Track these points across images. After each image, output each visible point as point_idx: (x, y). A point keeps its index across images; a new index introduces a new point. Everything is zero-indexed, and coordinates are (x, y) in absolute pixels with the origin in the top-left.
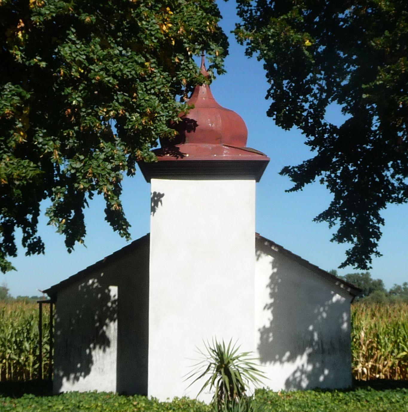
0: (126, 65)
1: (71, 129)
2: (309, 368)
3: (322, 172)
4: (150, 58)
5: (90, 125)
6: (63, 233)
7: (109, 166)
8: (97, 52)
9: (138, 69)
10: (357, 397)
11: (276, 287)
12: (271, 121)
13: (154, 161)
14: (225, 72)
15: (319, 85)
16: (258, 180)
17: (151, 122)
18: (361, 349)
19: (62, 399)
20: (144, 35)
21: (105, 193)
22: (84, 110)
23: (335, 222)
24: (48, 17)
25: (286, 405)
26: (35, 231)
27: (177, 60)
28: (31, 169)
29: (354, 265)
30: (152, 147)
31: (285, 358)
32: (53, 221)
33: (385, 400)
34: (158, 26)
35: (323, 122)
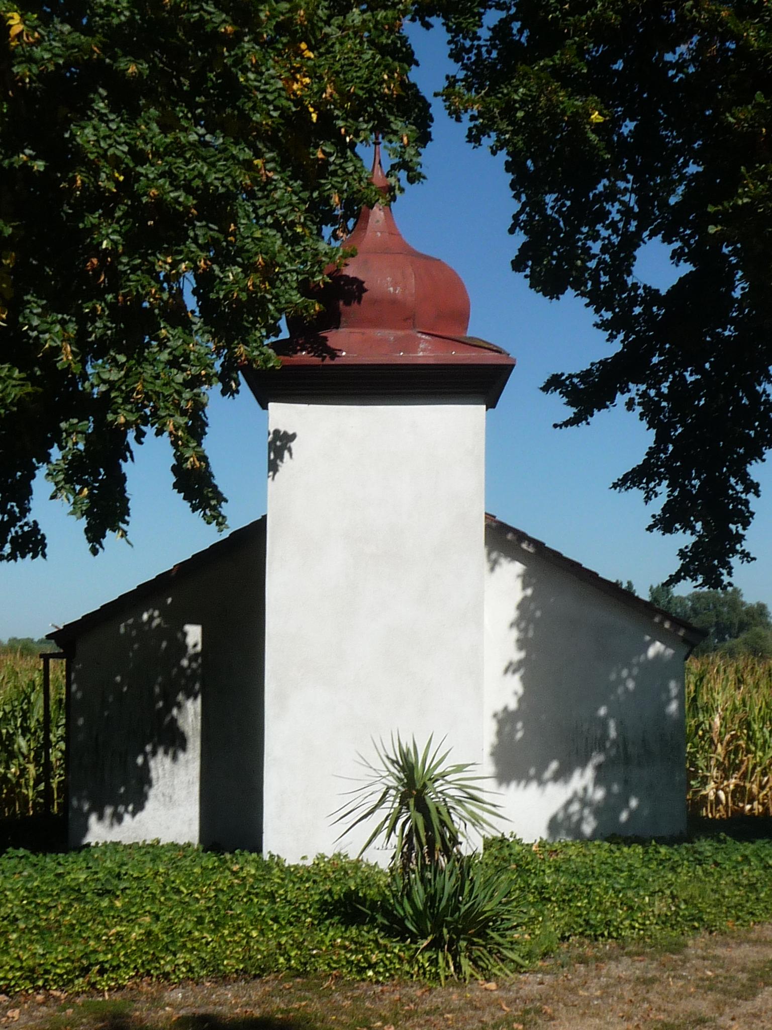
0: (212, 165)
1: (98, 300)
2: (599, 794)
3: (631, 386)
4: (264, 150)
5: (137, 291)
6: (83, 515)
7: (180, 378)
8: (152, 138)
9: (238, 173)
10: (697, 856)
11: (531, 626)
12: (521, 281)
13: (273, 366)
14: (424, 178)
15: (622, 203)
16: (491, 404)
17: (267, 284)
18: (714, 752)
19: (84, 860)
20: (251, 104)
21: (171, 433)
22: (125, 260)
23: (658, 489)
24: (48, 65)
25: (548, 871)
26: (25, 511)
27: (320, 155)
28: (14, 382)
29: (696, 580)
30: (268, 337)
31: (548, 774)
32: (63, 491)
33: (754, 861)
34: (277, 82)
35: (630, 281)
